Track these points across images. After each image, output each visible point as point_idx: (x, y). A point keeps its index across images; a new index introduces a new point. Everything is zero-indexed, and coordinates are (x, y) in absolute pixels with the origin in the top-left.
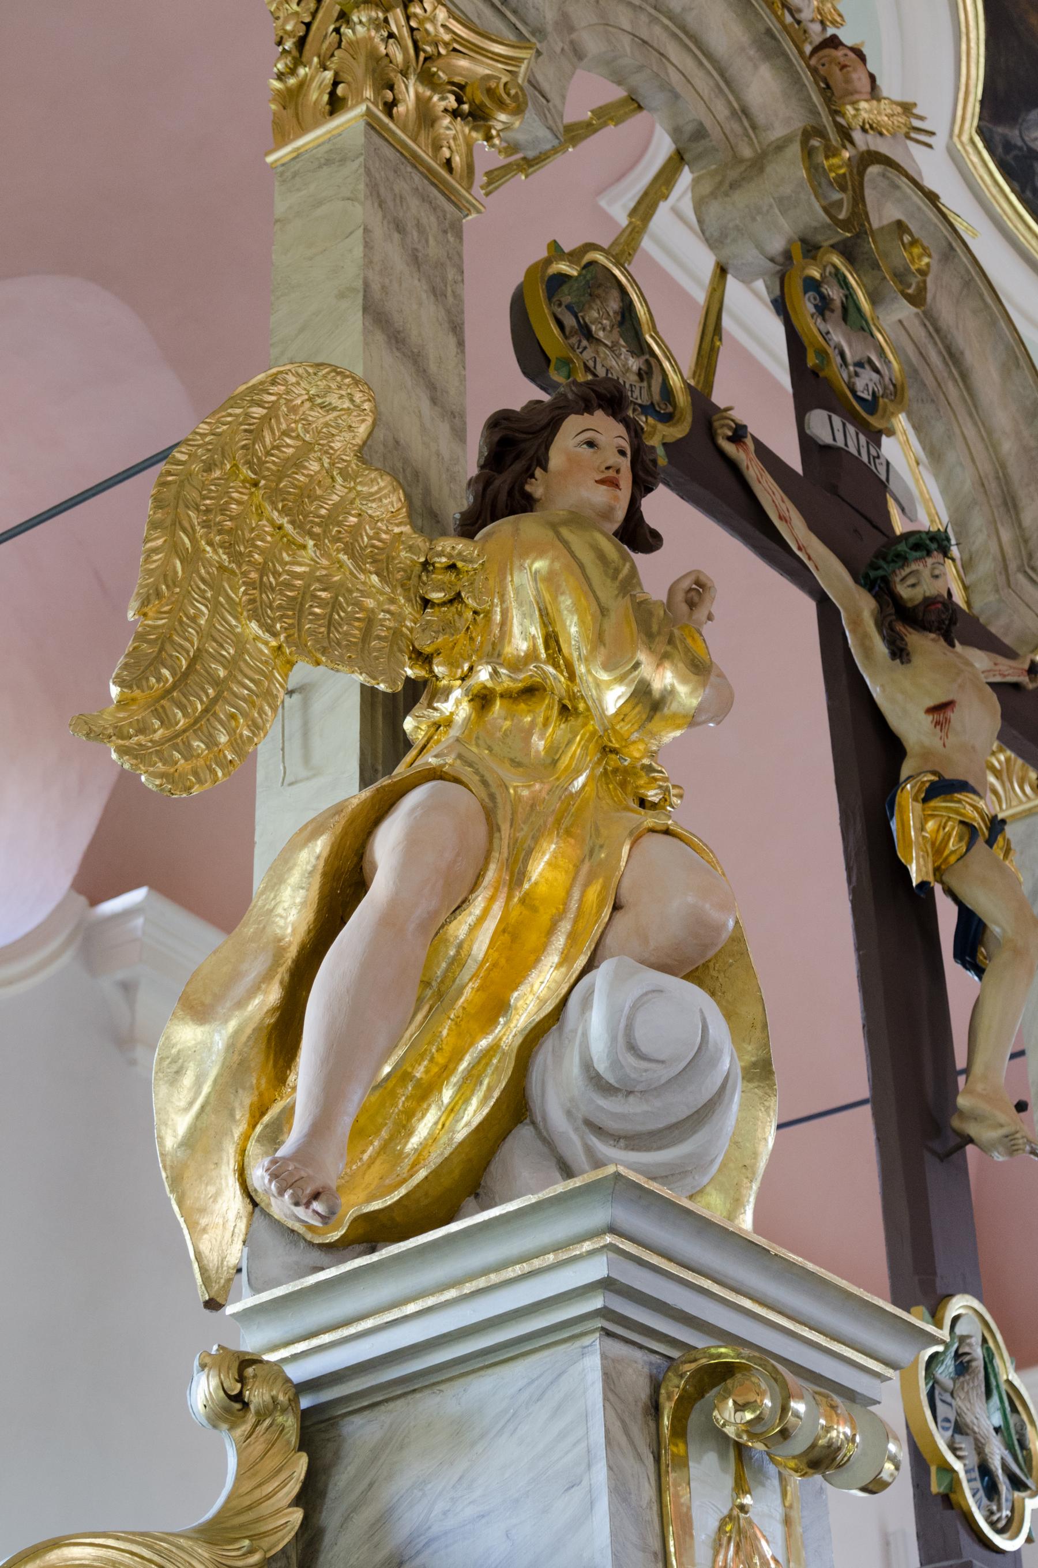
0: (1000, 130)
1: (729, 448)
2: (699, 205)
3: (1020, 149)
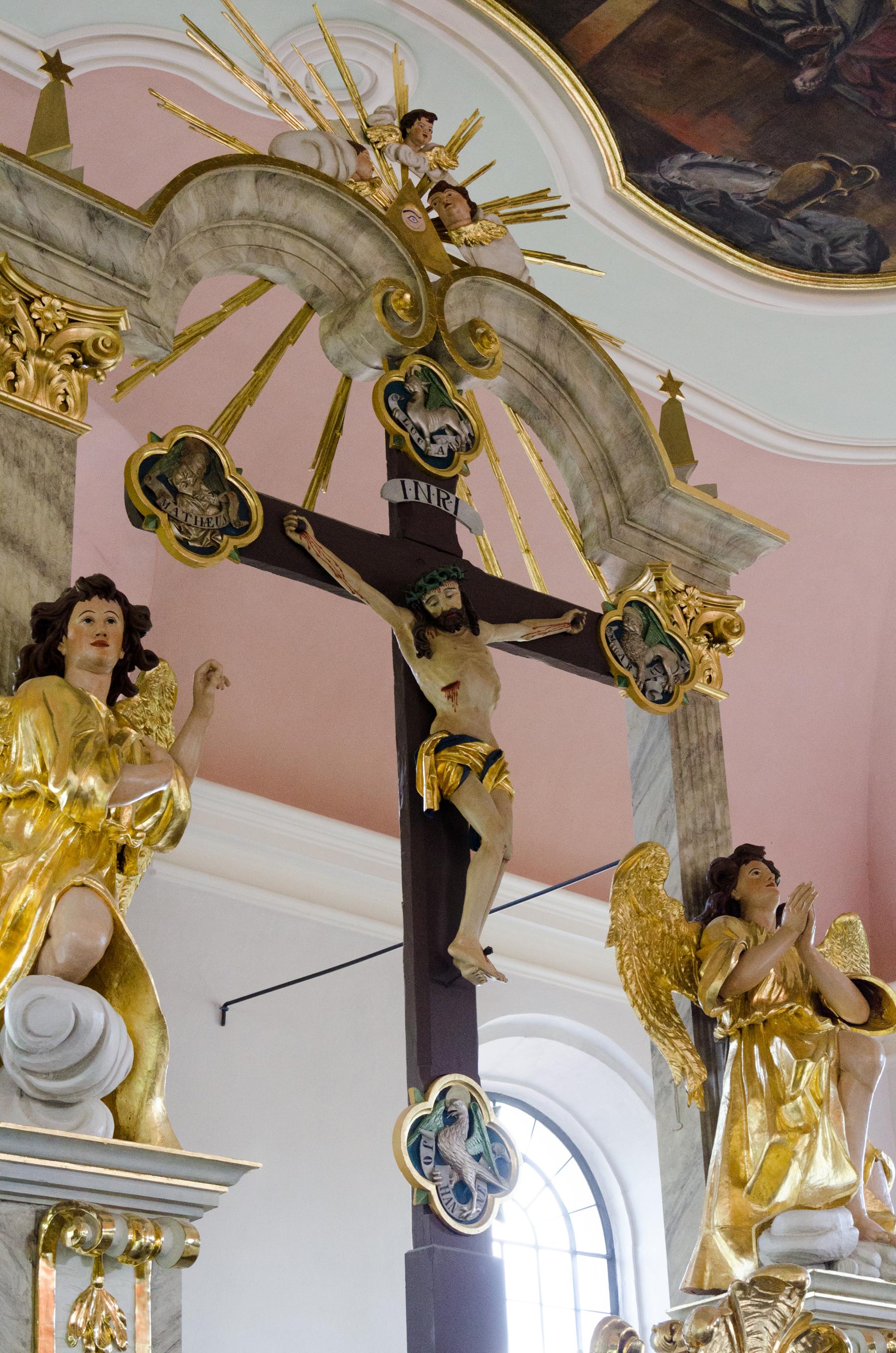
0: (645, 175)
1: (295, 537)
2: (323, 339)
3: (665, 184)
